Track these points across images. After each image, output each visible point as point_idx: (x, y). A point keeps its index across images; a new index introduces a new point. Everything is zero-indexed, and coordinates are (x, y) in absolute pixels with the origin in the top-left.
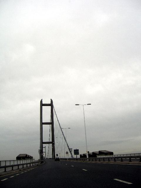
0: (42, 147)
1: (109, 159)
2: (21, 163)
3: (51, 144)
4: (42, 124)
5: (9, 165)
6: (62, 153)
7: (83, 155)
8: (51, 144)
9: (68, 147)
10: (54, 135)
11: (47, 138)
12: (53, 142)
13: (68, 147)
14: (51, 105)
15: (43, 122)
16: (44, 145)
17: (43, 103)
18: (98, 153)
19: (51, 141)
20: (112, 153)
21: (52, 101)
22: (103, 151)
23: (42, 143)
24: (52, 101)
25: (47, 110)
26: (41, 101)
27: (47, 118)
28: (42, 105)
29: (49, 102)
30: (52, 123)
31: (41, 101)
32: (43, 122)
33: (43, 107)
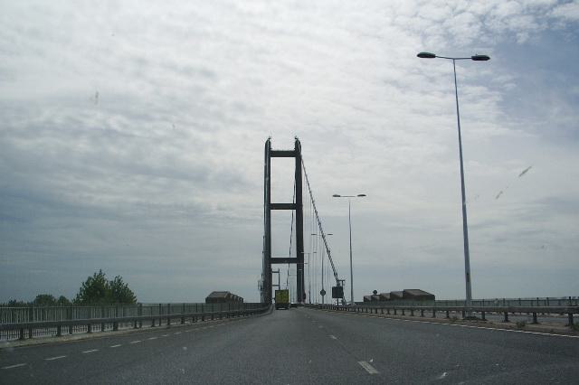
0: (268, 273)
1: (535, 314)
2: (112, 317)
3: (294, 266)
4: (270, 206)
5: (463, 297)
6: (318, 288)
7: (389, 297)
8: (294, 266)
9: (335, 274)
10: (302, 206)
11: (283, 245)
12: (299, 260)
13: (335, 274)
14: (296, 153)
15: (273, 201)
16: (274, 267)
17: (274, 147)
18: (401, 295)
19: (294, 255)
20: (432, 297)
21: (298, 144)
22: (411, 292)
23: (269, 260)
24: (298, 144)
25: (283, 169)
26: (268, 144)
27: (283, 191)
28: (270, 153)
29: (292, 148)
30: (297, 206)
31: (268, 144)
32: (273, 201)
33: (294, 255)
